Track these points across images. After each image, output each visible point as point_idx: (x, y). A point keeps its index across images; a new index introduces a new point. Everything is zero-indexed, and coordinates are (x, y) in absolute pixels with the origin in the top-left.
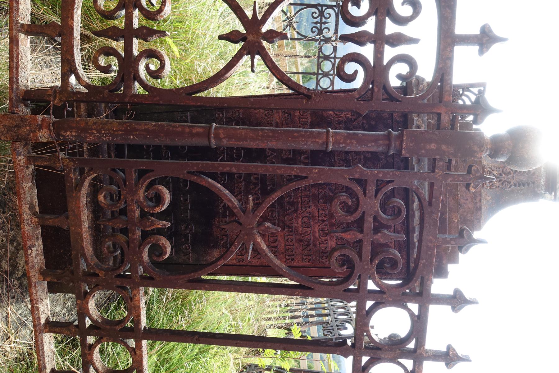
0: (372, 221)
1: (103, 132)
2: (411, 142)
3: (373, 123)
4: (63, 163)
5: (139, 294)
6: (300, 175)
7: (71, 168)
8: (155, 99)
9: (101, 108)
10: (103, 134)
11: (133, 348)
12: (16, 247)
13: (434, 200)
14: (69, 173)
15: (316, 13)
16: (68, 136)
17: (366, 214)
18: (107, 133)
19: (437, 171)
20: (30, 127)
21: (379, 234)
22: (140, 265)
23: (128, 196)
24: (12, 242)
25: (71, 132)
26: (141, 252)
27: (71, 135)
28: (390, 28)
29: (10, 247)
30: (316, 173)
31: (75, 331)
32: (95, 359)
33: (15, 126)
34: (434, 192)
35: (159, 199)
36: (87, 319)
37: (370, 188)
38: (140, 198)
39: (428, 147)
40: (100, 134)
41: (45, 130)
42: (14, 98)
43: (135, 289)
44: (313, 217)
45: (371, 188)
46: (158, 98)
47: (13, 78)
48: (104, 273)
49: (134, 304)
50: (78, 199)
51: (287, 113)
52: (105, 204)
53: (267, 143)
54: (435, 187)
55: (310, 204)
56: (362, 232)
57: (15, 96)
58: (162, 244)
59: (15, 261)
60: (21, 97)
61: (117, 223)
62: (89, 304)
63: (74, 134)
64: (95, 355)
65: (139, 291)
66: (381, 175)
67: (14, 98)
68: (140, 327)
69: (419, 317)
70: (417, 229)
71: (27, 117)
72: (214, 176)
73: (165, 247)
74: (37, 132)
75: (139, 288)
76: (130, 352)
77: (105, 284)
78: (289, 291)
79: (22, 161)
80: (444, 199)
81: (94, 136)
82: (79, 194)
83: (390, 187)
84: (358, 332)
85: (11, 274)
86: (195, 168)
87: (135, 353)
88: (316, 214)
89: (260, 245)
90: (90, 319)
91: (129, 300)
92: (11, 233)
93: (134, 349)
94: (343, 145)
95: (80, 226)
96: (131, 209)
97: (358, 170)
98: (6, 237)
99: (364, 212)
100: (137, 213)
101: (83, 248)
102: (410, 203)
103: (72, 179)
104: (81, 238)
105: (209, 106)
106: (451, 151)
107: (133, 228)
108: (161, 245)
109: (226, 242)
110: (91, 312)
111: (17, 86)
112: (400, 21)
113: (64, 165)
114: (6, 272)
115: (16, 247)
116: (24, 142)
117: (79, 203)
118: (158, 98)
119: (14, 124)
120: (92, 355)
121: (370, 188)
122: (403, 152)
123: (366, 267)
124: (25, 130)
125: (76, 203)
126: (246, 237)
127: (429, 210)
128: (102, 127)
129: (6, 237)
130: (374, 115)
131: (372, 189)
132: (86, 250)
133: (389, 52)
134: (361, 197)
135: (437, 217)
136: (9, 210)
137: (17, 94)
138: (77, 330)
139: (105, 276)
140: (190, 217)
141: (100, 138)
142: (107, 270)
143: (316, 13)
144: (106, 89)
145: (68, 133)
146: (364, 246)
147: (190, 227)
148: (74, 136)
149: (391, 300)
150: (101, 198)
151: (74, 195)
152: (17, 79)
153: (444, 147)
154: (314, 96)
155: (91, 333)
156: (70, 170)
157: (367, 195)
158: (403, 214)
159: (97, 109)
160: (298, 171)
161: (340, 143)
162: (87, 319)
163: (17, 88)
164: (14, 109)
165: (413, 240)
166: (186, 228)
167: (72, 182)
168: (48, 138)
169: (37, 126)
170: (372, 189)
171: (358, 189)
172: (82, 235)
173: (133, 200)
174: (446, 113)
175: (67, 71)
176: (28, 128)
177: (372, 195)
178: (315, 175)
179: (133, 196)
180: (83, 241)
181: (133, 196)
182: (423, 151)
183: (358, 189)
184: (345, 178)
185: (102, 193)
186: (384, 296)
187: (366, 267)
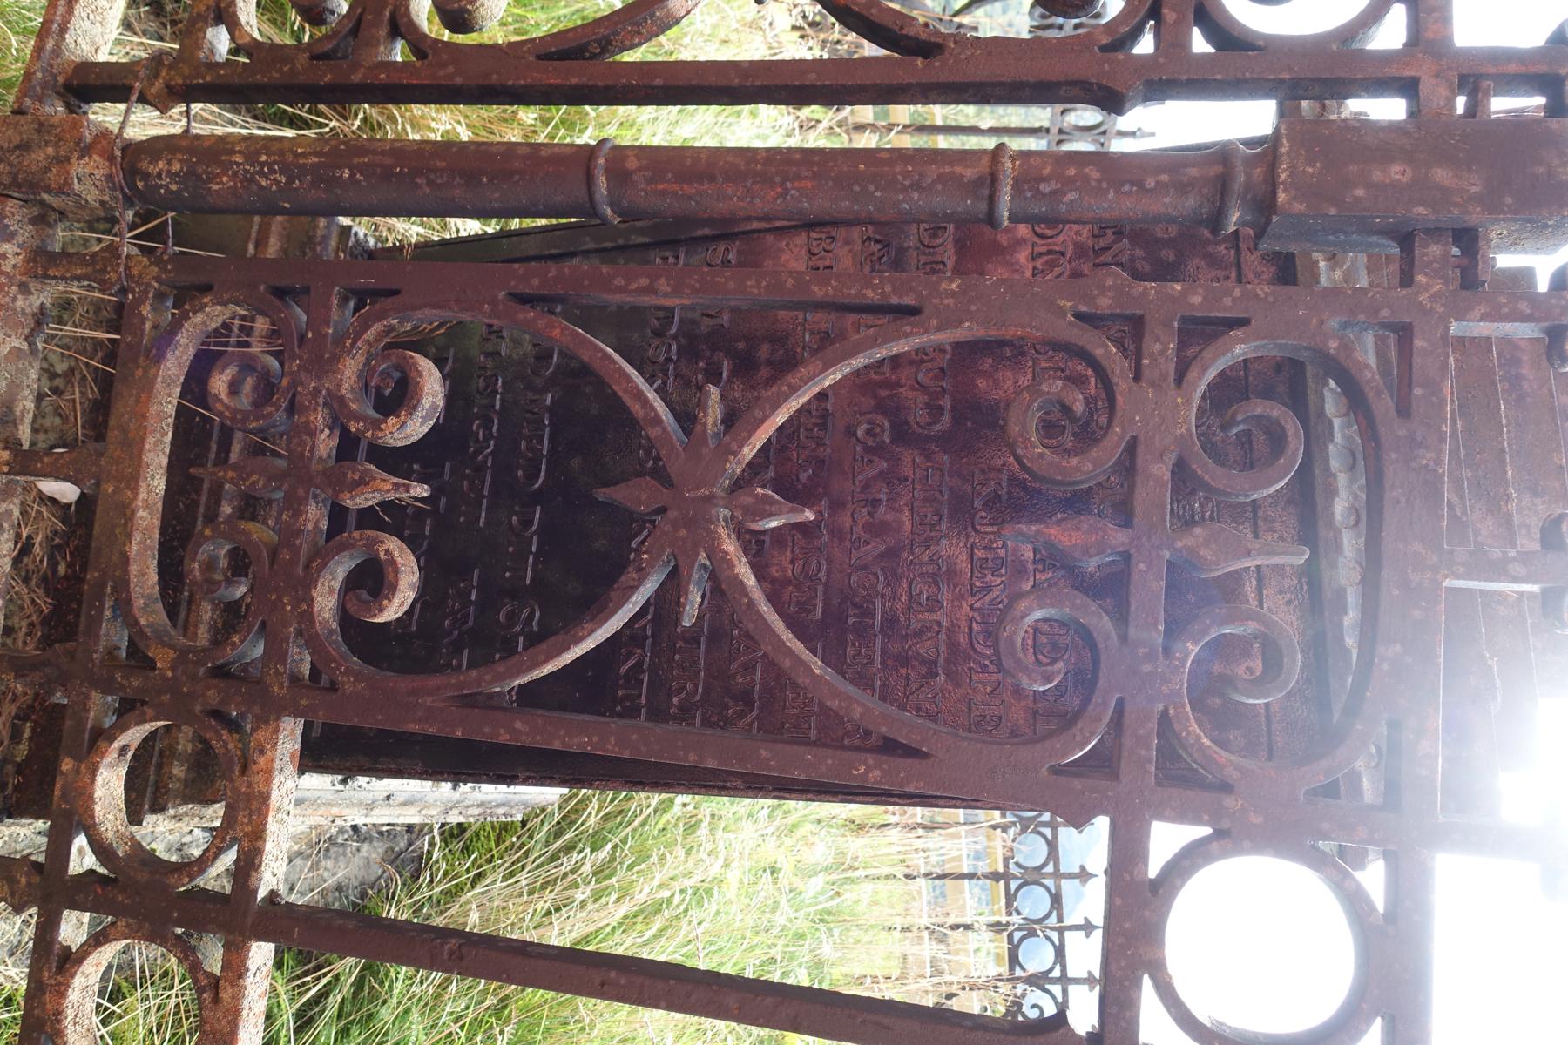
0: (1168, 476)
1: (264, 158)
2: (1311, 163)
3: (1169, 255)
4: (127, 268)
5: (274, 746)
6: (894, 300)
7: (148, 285)
8: (441, 73)
9: (326, 248)
10: (263, 164)
11: (210, 975)
13: (1418, 391)
14: (138, 302)
16: (159, 176)
17: (1140, 450)
18: (275, 162)
19: (1421, 278)
20: (56, 146)
21: (1197, 531)
23: (303, 376)
25: (169, 163)
26: (310, 582)
27: (169, 171)
30: (953, 294)
31: (29, 884)
32: (70, 1013)
33: (17, 147)
34: (1417, 360)
35: (396, 396)
36: (81, 841)
37: (1158, 347)
38: (339, 386)
39: (1377, 176)
40: (252, 165)
41: (96, 157)
42: (39, 75)
43: (267, 723)
44: (952, 572)
45: (1161, 347)
46: (451, 69)
47: (52, 22)
48: (172, 654)
49: (250, 785)
50: (148, 387)
51: (877, 241)
52: (227, 407)
53: (782, 184)
54: (1419, 343)
55: (944, 526)
56: (1127, 523)
57: (43, 70)
58: (387, 552)
60: (61, 79)
61: (253, 472)
62: (99, 780)
63: (176, 167)
64: (73, 996)
65: (276, 731)
66: (1196, 300)
67: (39, 75)
68: (253, 882)
69: (1391, 916)
70: (1352, 598)
71: (55, 121)
72: (592, 318)
73: (393, 563)
74: (73, 161)
75: (278, 719)
76: (200, 991)
77: (166, 698)
78: (713, 80)
79: (12, 261)
80: (1455, 499)
81: (235, 174)
82: (152, 372)
83: (1239, 349)
84: (1113, 967)
86: (536, 282)
87: (216, 1000)
88: (963, 565)
89: (731, 565)
90: (91, 842)
91: (237, 769)
93: (215, 982)
94: (1053, 185)
95: (132, 480)
96: (308, 422)
97: (1109, 282)
99: (1132, 448)
100: (326, 444)
101: (125, 559)
102: (1320, 500)
103: (143, 320)
104: (126, 524)
106: (1474, 189)
107: (301, 492)
108: (382, 556)
109: (639, 664)
110: (98, 811)
111: (58, 46)
113: (129, 277)
116: (36, 211)
117: (149, 400)
118: (451, 69)
119: (16, 140)
120: (63, 995)
121: (1158, 347)
122: (1281, 197)
123: (1147, 668)
124: (39, 156)
125: (138, 401)
126: (683, 533)
127: (1402, 433)
128: (264, 147)
130: (1173, 231)
131: (1163, 352)
132: (134, 568)
134: (1123, 385)
135: (1438, 462)
137: (51, 66)
138: (36, 879)
139: (173, 669)
140: (532, 579)
141: (252, 180)
142: (183, 653)
144: (304, 51)
145: (161, 165)
146: (1135, 577)
147: (525, 613)
148: (177, 174)
149: (1258, 820)
150: (219, 384)
151: (139, 372)
152: (63, 29)
153: (1442, 175)
154: (952, 45)
155: (80, 898)
156: (146, 292)
157: (1146, 373)
158: (1292, 446)
159: (313, 250)
160: (888, 288)
161: (1042, 179)
162: (81, 841)
163: (57, 52)
164: (28, 102)
165: (1340, 638)
166: (512, 617)
167: (143, 331)
168: (102, 191)
169: (77, 144)
170: (1163, 352)
171: (1106, 351)
172: (133, 513)
173: (317, 391)
174: (1437, 76)
175: (208, 8)
176: (50, 150)
177: (1164, 377)
178: (950, 301)
179: (319, 378)
180: (129, 536)
181: (319, 378)
182: (1360, 192)
183: (1106, 351)
184: (1061, 312)
185: (225, 368)
186: (1229, 802)
187: (1147, 668)
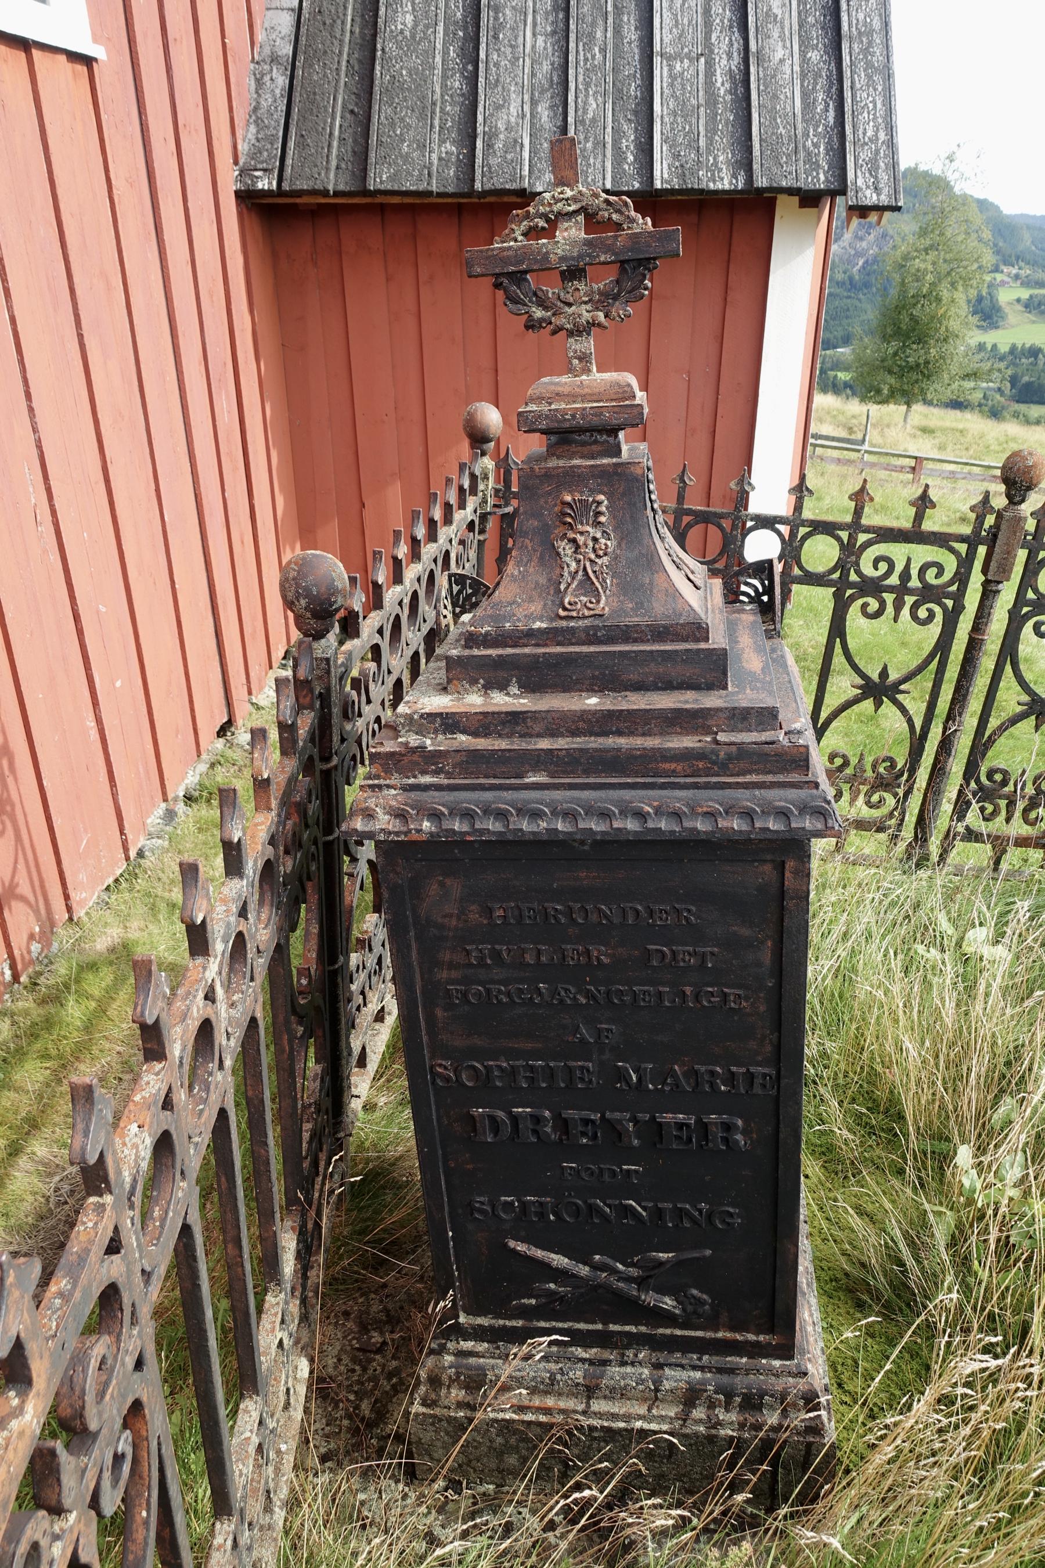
12: (394, 1387)
15: (865, 606)
22: (64, 1277)
24: (390, 1376)
28: (910, 600)
29: (383, 1382)
59: (385, 1406)
85: (370, 1425)
92: (394, 1363)
98: (384, 1366)
105: (314, 192)
112: (915, 607)
114: (363, 1419)
115: (394, 1387)
129: (384, 1366)
133: (889, 598)
136: (401, 1330)
143: (865, 606)
